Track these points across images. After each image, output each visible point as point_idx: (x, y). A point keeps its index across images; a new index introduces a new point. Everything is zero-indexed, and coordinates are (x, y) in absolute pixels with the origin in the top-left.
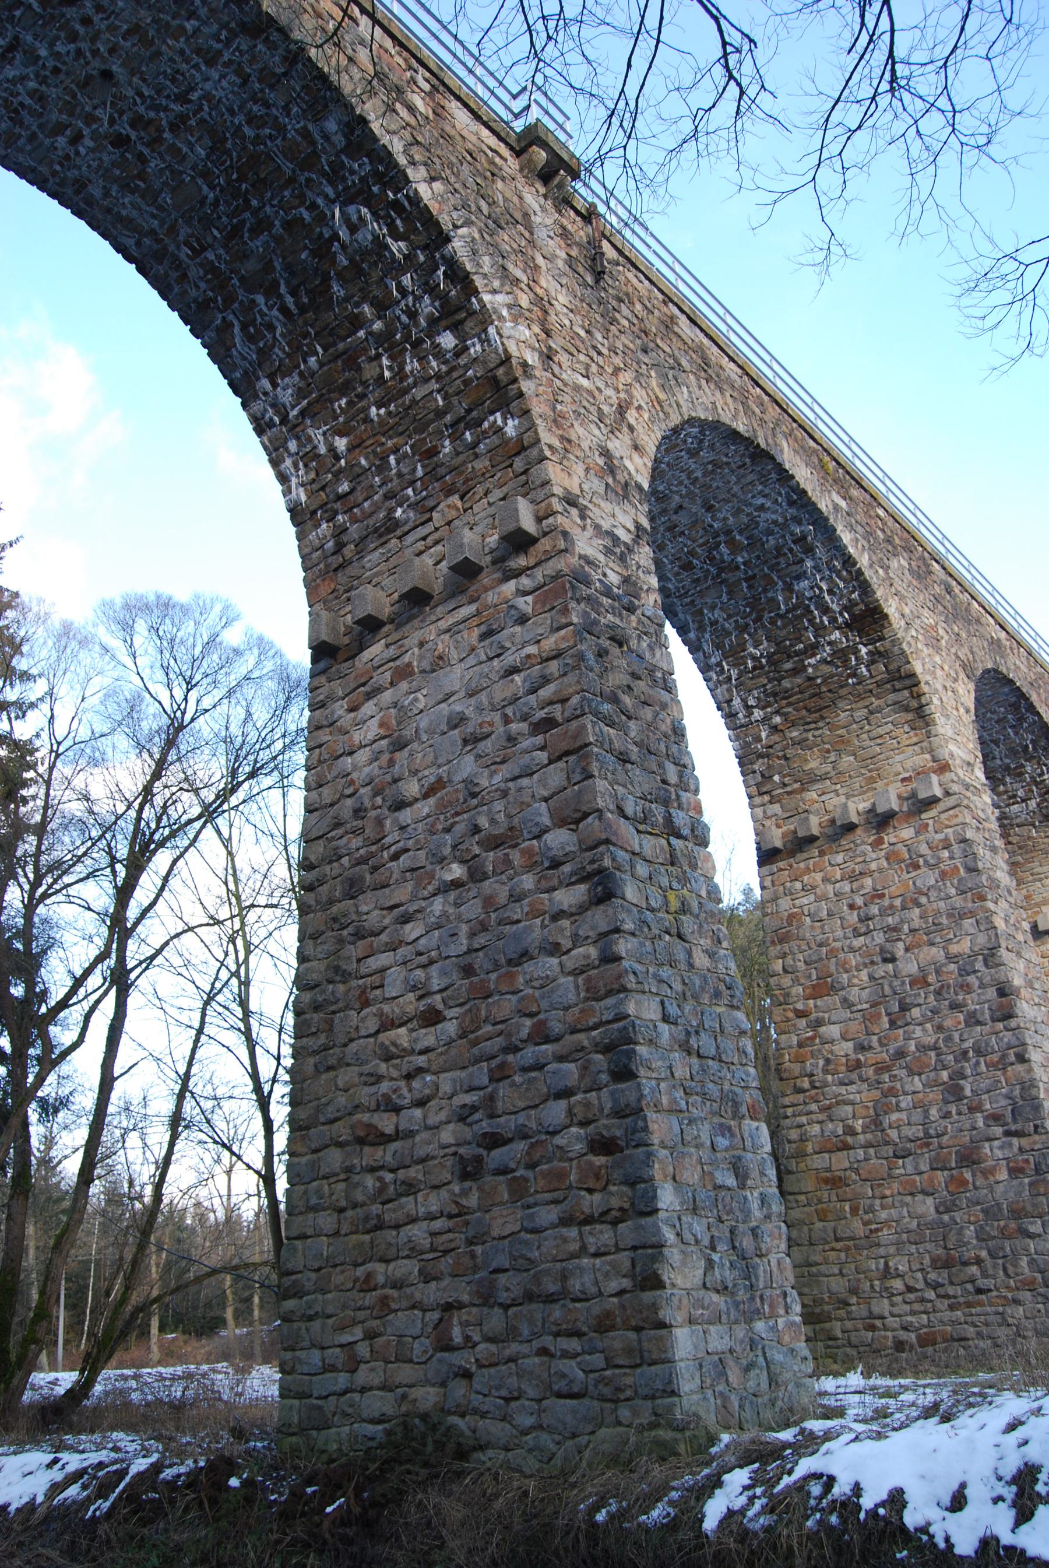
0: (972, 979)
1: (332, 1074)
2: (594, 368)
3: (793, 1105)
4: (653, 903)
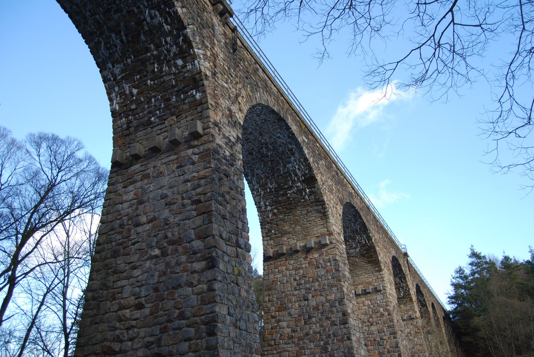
0: (334, 309)
1: (97, 325)
2: (229, 81)
3: (267, 351)
4: (229, 271)
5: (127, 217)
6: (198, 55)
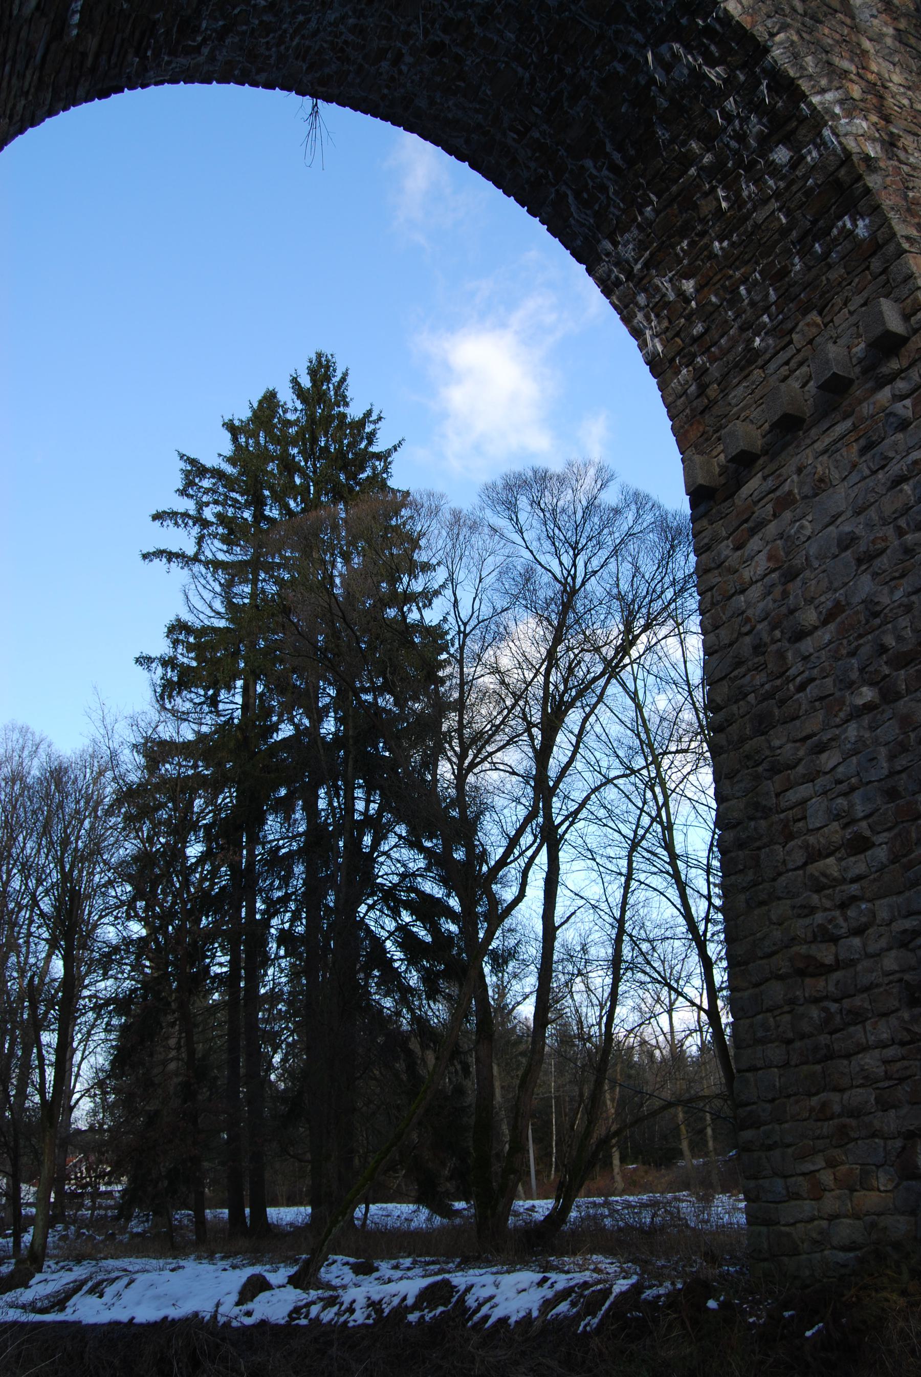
5: (766, 623)
6: (828, 111)
